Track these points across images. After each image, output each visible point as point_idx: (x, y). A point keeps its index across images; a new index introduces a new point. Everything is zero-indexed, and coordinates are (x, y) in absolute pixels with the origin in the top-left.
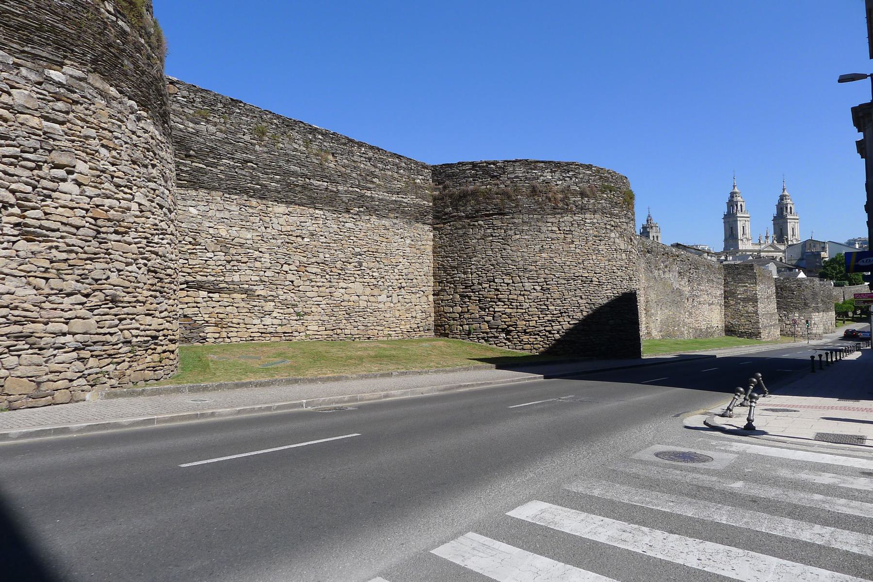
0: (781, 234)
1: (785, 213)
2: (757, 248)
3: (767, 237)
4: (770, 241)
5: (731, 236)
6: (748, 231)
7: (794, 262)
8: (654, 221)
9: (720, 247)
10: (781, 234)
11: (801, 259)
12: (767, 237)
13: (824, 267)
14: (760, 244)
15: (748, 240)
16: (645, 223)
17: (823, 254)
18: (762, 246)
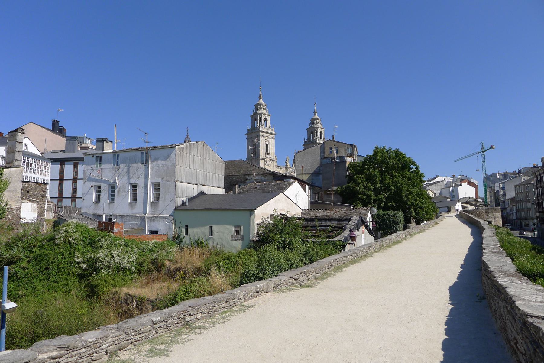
1: (315, 137)
6: (272, 150)
14: (286, 167)
18: (289, 170)
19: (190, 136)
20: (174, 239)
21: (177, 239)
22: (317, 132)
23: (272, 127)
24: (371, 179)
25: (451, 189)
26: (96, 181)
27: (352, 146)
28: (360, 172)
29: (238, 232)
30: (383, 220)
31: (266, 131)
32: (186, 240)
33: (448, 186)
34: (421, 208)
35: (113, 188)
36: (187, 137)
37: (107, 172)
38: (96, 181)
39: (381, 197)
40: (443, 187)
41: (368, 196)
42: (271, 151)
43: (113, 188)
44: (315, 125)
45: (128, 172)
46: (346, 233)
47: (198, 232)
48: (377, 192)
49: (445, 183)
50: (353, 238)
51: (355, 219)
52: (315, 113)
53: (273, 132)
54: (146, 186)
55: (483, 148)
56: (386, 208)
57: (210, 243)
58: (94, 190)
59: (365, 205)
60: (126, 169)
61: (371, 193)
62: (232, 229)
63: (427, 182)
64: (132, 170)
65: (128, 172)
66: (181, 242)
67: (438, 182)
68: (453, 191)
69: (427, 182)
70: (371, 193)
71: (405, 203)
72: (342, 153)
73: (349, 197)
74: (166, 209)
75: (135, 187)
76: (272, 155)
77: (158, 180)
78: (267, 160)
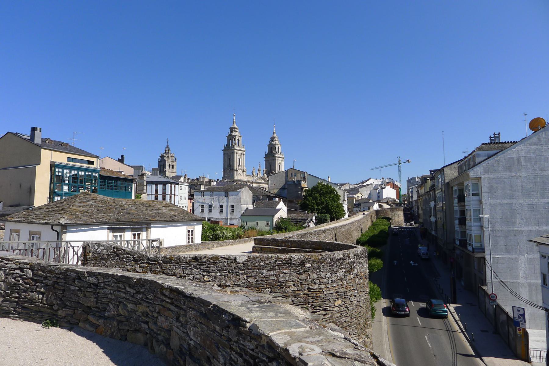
0: (270, 168)
1: (274, 152)
2: (250, 179)
3: (259, 171)
4: (261, 175)
5: (229, 167)
6: (243, 163)
7: (276, 191)
8: (172, 151)
9: (219, 175)
10: (270, 168)
11: (283, 189)
12: (259, 171)
13: (305, 197)
14: (253, 176)
15: (243, 171)
16: (163, 152)
17: (304, 184)
18: (255, 178)
19: (169, 146)
20: (241, 227)
21: (242, 227)
22: (275, 147)
23: (243, 145)
24: (315, 199)
25: (377, 190)
26: (201, 203)
27: (304, 172)
28: (310, 195)
29: (268, 224)
30: (320, 219)
31: (239, 149)
32: (246, 227)
33: (376, 188)
34: (338, 213)
35: (210, 206)
36: (167, 147)
37: (207, 199)
38: (201, 203)
39: (319, 207)
40: (372, 189)
41: (314, 207)
42: (242, 164)
43: (210, 206)
44: (274, 142)
45: (219, 200)
46: (306, 224)
47: (251, 224)
48: (318, 205)
49: (374, 185)
50: (309, 226)
51: (309, 219)
52: (274, 133)
53: (244, 149)
54: (227, 206)
55: (399, 161)
56: (321, 213)
57: (257, 228)
58: (200, 207)
59: (312, 212)
60: (217, 199)
61: (315, 205)
62: (266, 223)
63: (361, 184)
64: (220, 200)
65: (219, 200)
66: (244, 228)
67: (368, 185)
68: (379, 193)
69: (361, 184)
70: (315, 205)
71: (330, 210)
72: (299, 178)
73: (304, 207)
74: (237, 214)
75: (221, 207)
76: (243, 168)
77: (233, 204)
78: (239, 171)
